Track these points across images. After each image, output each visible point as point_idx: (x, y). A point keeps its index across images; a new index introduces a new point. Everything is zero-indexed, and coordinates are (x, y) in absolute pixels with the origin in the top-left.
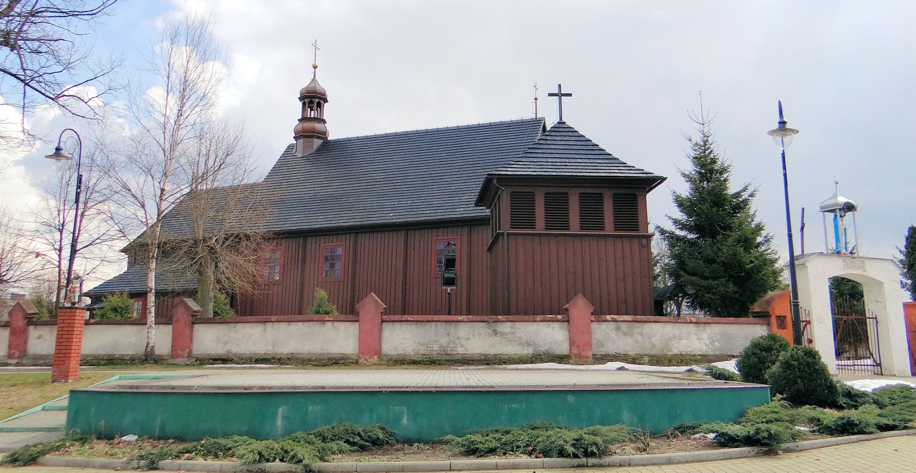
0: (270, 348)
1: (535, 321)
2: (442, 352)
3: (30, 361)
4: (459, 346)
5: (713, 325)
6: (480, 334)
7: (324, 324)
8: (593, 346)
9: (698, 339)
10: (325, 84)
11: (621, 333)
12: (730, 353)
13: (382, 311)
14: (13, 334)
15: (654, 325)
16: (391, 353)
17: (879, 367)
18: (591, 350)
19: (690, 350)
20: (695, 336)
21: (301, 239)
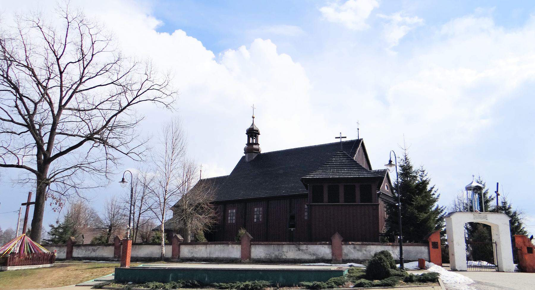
0: (208, 255)
2: (276, 258)
7: (228, 245)
8: (343, 255)
10: (258, 126)
12: (408, 259)
13: (251, 240)
14: (115, 248)
16: (255, 258)
18: (342, 257)
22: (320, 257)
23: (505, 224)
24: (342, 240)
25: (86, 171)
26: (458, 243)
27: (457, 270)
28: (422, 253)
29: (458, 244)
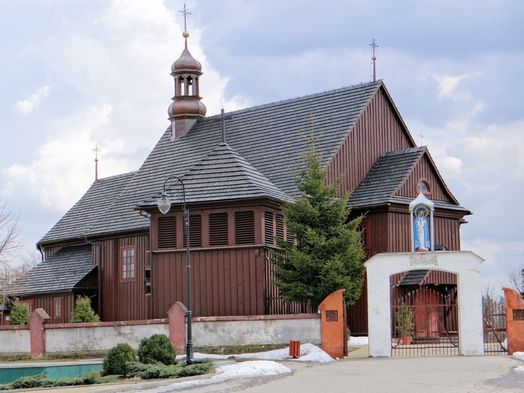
1: (147, 324)
2: (85, 350)
5: (278, 321)
6: (109, 335)
7: (15, 331)
9: (266, 332)
11: (208, 330)
13: (43, 321)
15: (233, 323)
17: (457, 349)
19: (259, 341)
20: (263, 330)
21: (141, 237)
23: (472, 270)
26: (377, 310)
27: (463, 355)
28: (310, 330)
29: (376, 311)
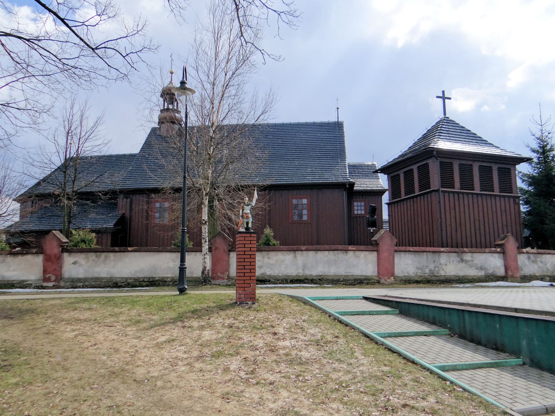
0: (301, 271)
2: (431, 275)
3: (68, 284)
4: (441, 269)
6: (453, 261)
7: (346, 252)
22: (490, 272)
24: (517, 246)
25: (41, 54)
